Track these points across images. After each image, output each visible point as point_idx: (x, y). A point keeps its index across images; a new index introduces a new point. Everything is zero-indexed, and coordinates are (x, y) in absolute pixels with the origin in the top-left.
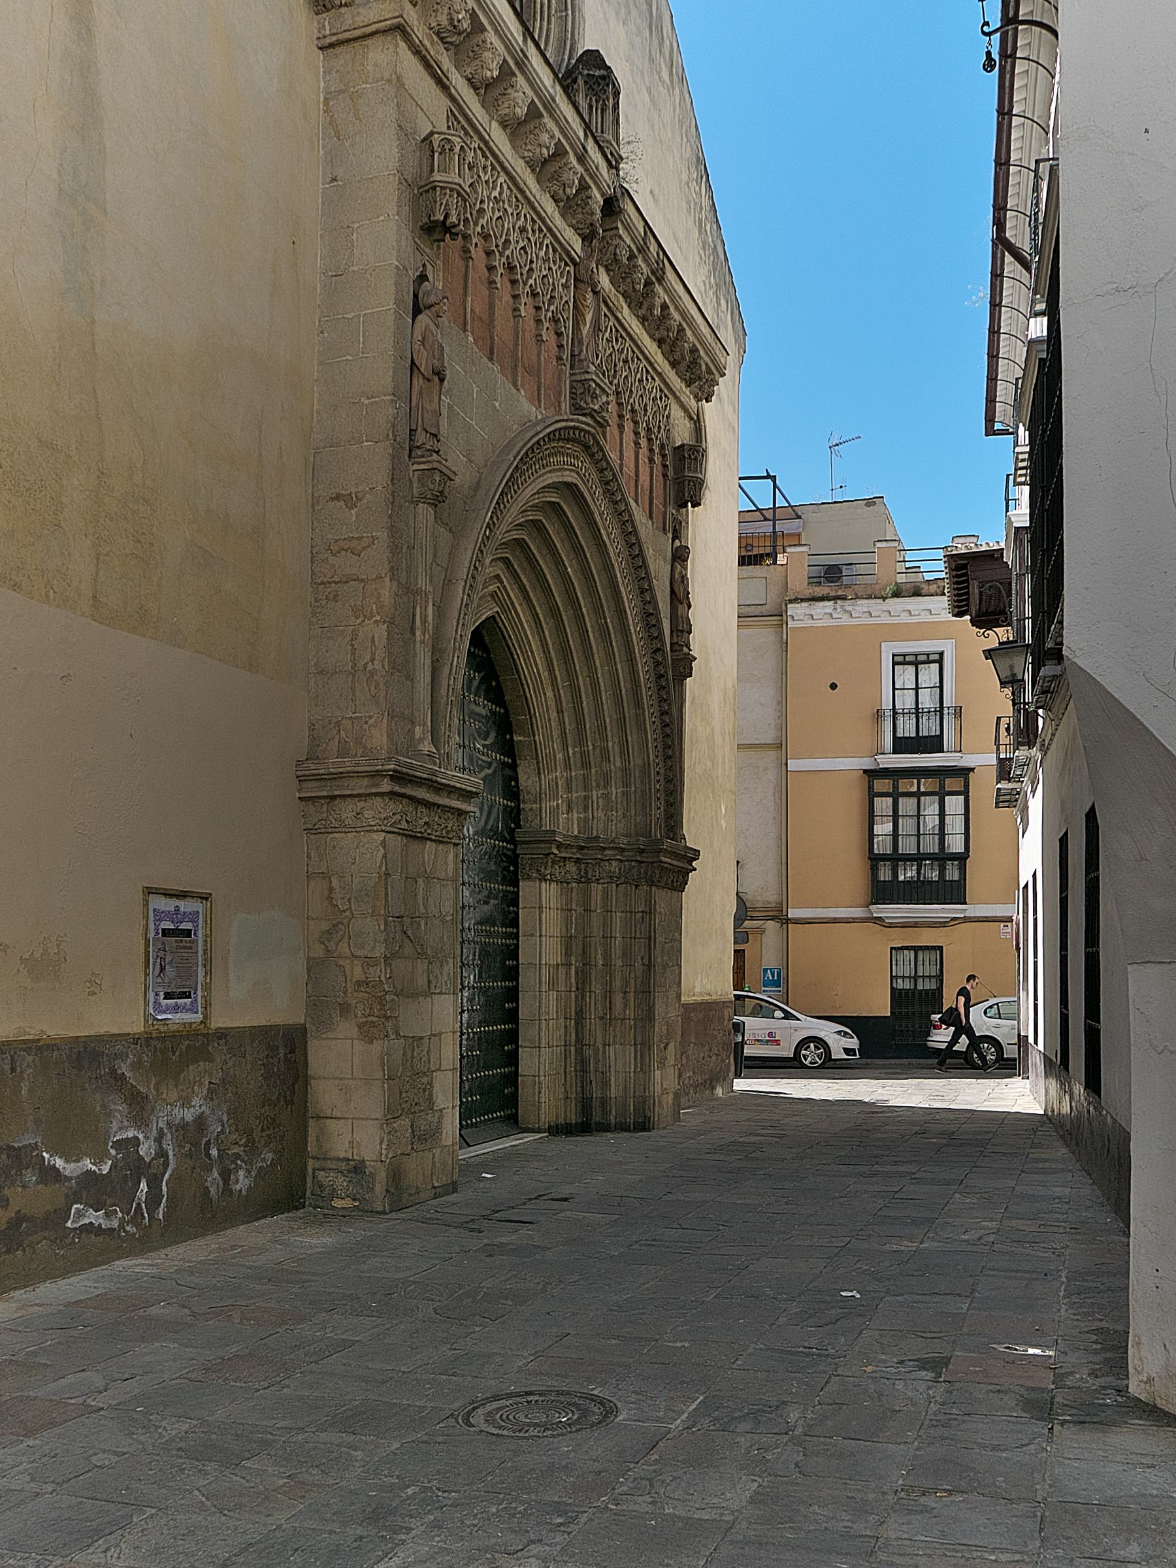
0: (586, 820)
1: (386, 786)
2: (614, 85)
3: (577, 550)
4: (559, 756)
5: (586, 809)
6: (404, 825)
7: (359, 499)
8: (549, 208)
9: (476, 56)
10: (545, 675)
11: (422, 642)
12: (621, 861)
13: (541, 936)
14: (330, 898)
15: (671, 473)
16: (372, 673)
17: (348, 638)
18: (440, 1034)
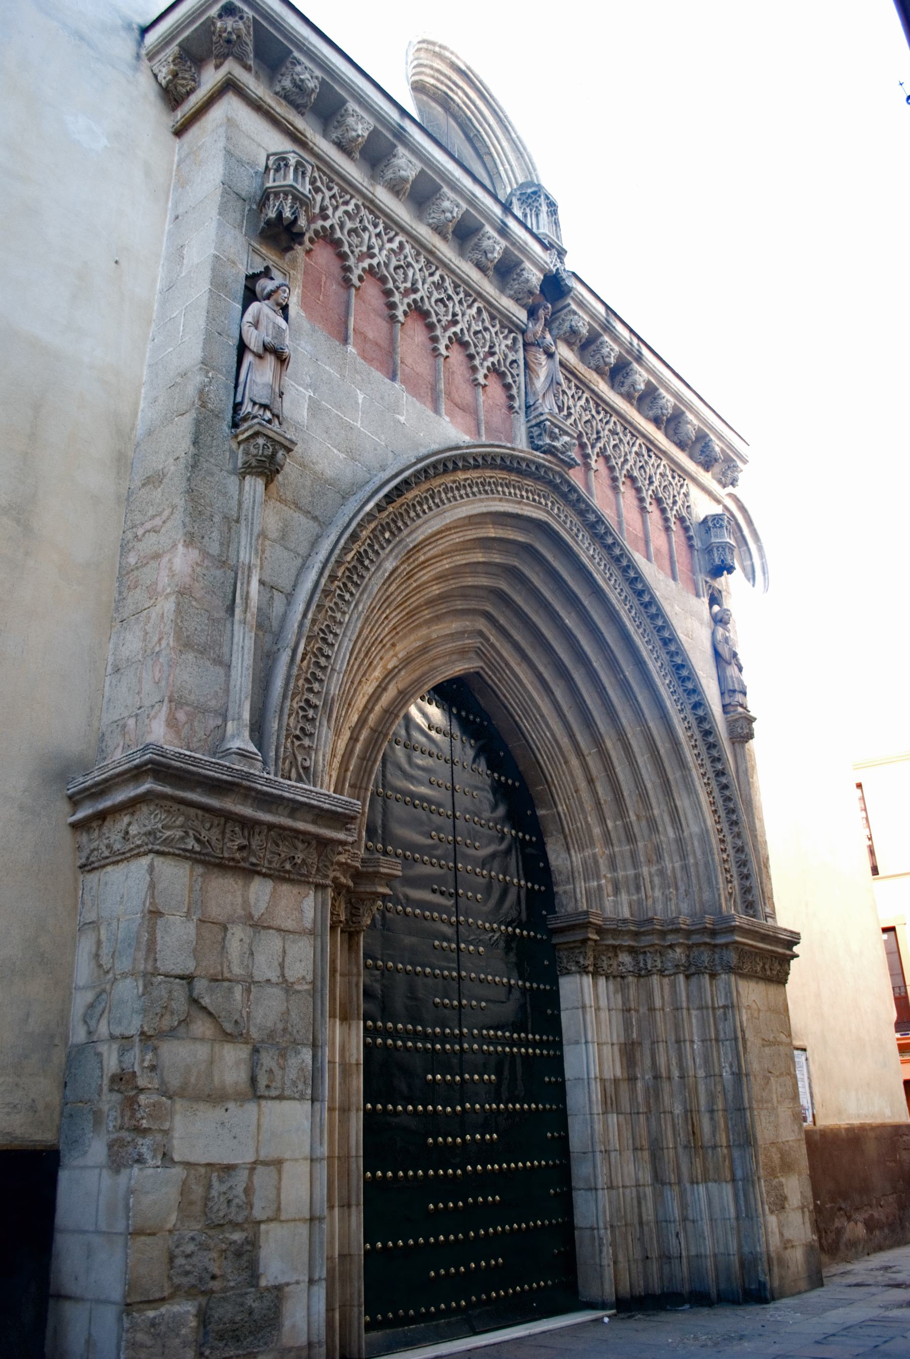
0: (640, 902)
2: (547, 198)
3: (573, 600)
4: (597, 831)
5: (638, 889)
6: (191, 843)
7: (164, 476)
8: (475, 275)
9: (341, 124)
11: (244, 622)
13: (586, 1042)
14: (97, 956)
15: (697, 543)
18: (278, 1163)
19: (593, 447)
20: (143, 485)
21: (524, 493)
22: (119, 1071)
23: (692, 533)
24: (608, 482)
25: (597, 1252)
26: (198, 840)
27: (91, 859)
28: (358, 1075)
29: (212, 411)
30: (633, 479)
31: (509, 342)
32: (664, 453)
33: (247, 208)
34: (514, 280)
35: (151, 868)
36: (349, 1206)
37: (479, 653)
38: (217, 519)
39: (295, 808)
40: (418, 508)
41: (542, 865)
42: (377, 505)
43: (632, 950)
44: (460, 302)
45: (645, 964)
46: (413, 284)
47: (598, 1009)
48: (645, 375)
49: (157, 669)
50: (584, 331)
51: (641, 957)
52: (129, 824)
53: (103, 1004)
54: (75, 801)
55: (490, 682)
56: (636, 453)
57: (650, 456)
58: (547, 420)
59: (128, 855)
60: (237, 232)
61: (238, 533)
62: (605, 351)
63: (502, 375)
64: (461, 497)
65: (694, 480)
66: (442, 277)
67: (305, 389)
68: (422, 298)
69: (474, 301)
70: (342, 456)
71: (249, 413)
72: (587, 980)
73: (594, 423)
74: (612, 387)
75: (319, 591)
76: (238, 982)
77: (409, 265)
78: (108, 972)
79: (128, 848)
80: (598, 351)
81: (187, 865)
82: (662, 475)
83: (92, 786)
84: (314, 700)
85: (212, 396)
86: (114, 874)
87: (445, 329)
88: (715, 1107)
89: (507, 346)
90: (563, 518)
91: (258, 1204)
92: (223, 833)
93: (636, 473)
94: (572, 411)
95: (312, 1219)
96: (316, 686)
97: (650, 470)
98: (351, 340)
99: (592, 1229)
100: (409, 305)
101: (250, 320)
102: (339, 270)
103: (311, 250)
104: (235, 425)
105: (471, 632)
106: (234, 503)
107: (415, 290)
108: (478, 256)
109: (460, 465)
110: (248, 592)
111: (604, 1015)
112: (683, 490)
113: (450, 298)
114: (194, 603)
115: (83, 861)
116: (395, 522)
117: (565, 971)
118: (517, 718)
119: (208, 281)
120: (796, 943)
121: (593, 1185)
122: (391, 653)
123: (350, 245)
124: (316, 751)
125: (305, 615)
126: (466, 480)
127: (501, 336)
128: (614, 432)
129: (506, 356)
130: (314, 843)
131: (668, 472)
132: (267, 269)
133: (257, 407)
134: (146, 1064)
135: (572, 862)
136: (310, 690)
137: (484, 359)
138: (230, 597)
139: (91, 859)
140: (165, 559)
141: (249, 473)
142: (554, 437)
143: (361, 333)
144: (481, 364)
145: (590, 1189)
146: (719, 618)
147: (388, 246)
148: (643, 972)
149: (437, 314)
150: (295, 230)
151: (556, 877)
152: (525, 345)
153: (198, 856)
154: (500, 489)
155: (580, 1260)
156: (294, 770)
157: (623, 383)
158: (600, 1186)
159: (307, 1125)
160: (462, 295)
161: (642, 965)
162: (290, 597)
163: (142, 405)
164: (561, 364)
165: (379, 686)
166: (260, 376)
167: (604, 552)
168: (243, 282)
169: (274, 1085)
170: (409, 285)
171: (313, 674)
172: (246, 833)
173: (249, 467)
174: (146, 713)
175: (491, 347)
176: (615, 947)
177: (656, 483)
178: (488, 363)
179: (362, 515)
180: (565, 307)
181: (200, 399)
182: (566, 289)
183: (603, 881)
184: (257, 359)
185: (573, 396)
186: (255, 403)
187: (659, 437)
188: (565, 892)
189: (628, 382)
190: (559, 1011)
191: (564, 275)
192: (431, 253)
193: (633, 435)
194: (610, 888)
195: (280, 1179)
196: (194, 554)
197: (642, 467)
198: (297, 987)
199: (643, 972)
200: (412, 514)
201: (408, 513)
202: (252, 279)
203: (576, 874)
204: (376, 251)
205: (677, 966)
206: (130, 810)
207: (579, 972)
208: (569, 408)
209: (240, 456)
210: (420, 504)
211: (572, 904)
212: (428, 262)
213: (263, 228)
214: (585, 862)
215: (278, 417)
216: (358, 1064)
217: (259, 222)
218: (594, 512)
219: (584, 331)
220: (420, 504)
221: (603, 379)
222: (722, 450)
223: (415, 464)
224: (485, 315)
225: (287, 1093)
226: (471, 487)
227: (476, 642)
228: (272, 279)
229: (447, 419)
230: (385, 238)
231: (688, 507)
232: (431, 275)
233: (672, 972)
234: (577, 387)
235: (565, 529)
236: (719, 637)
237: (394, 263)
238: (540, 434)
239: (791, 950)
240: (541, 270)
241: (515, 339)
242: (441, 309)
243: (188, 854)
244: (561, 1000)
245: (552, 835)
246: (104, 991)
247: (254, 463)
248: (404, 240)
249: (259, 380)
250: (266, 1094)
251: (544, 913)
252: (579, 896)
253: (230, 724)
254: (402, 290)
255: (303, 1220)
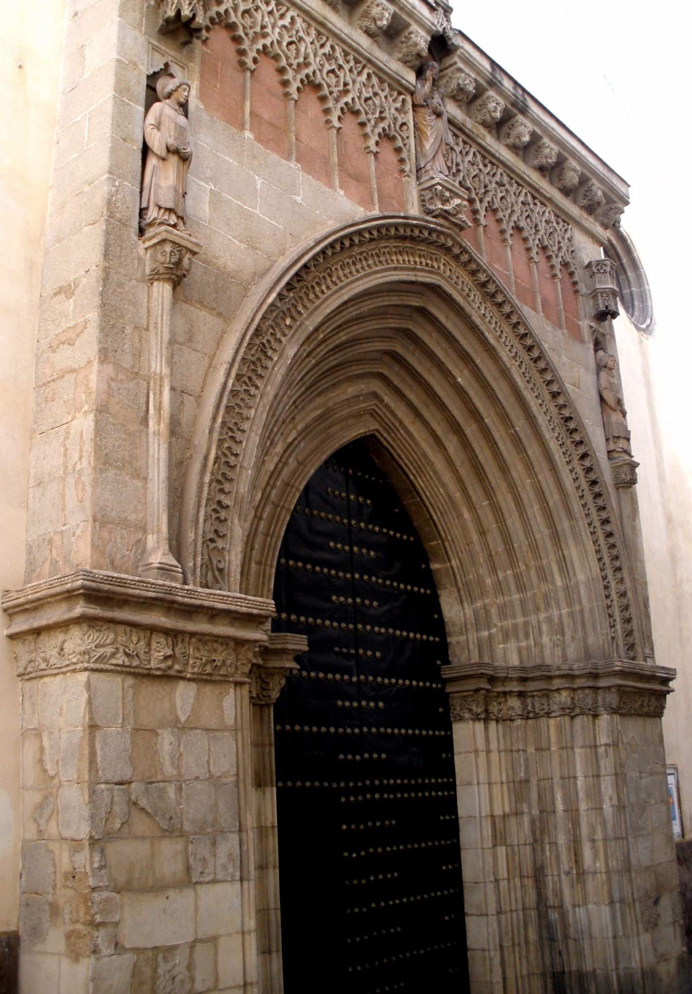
1: (80, 609)
5: (527, 636)
6: (120, 659)
7: (76, 286)
10: (458, 495)
12: (574, 690)
13: (478, 784)
14: (41, 761)
16: (80, 473)
17: (62, 439)
19: (481, 201)
20: (55, 294)
21: (417, 260)
22: (71, 869)
23: (576, 278)
24: (497, 235)
25: (488, 971)
26: (127, 655)
27: (29, 670)
28: (273, 835)
29: (120, 220)
30: (518, 229)
31: (398, 105)
32: (550, 200)
33: (146, 5)
34: (402, 43)
35: (88, 686)
36: (270, 953)
37: (373, 414)
38: (128, 330)
39: (213, 614)
40: (317, 289)
41: (436, 616)
42: (279, 294)
43: (521, 695)
44: (351, 70)
45: (533, 707)
46: (305, 58)
47: (488, 752)
48: (531, 127)
49: (80, 486)
50: (471, 88)
51: (529, 701)
52: (64, 641)
53: (51, 806)
54: (11, 612)
55: (385, 443)
56: (523, 203)
57: (535, 204)
58: (438, 184)
59: (64, 670)
60: (136, 33)
61: (148, 341)
62: (492, 105)
63: (392, 139)
64: (357, 271)
65: (578, 224)
66: (332, 47)
67: (207, 183)
68: (314, 72)
69: (364, 67)
70: (243, 246)
71: (155, 219)
72: (480, 726)
73: (482, 177)
74: (498, 138)
75: (227, 393)
76: (170, 782)
77: (301, 39)
78: (53, 778)
79: (64, 664)
80: (484, 105)
81: (119, 679)
82: (547, 222)
83: (26, 603)
84: (226, 501)
85: (119, 204)
86: (53, 684)
87: (337, 100)
88: (596, 837)
89: (396, 109)
90: (455, 279)
91: (199, 977)
92: (149, 644)
93: (522, 224)
94: (461, 168)
95: (245, 985)
96: (227, 486)
97: (535, 216)
98: (247, 126)
99: (484, 950)
100: (302, 81)
101: (153, 122)
102: (234, 54)
103: (207, 39)
104: (141, 232)
105: (366, 395)
106: (143, 312)
107: (307, 65)
108: (367, 23)
109: (357, 241)
110: (160, 403)
111: (494, 757)
112: (568, 235)
113: (340, 67)
114: (111, 420)
115: (21, 670)
116: (295, 306)
117: (458, 718)
118: (412, 477)
119: (112, 87)
120: (672, 679)
121: (484, 912)
122: (291, 426)
123: (244, 28)
124: (229, 552)
125: (214, 419)
126: (361, 253)
127: (390, 100)
128: (500, 184)
129: (396, 119)
130: (232, 644)
131: (553, 218)
132: (167, 65)
133: (162, 211)
134: (96, 865)
135: (465, 614)
136: (222, 491)
137: (375, 126)
138: (144, 408)
139: (29, 670)
140: (81, 376)
141: (157, 280)
142: (446, 201)
143: (257, 115)
144: (373, 131)
145: (482, 915)
146: (603, 364)
147: (280, 23)
148: (531, 715)
149: (329, 86)
150: (193, 26)
151: (449, 628)
152: (414, 106)
153: (128, 669)
154: (394, 258)
155: (472, 978)
156: (210, 574)
157: (509, 134)
158: (489, 913)
159: (237, 902)
160: (352, 63)
161: (530, 708)
162: (199, 399)
163: (50, 210)
164: (450, 122)
165: (280, 461)
166: (164, 179)
167: (495, 309)
168: (144, 82)
169: (207, 871)
170: (301, 60)
171: (224, 474)
172: (170, 643)
173: (157, 274)
174: (79, 553)
175: (381, 112)
176: (505, 693)
177: (542, 232)
178: (379, 130)
179: (265, 307)
180: (452, 65)
181: (108, 210)
182: (453, 48)
183: (494, 630)
184: (161, 161)
185: (461, 152)
186: (160, 208)
187: (543, 184)
188: (458, 643)
189: (514, 133)
190: (453, 754)
191: (451, 34)
192: (322, 24)
193: (519, 185)
194: (500, 636)
195: (216, 954)
196: (109, 369)
197: (528, 216)
198: (224, 780)
199: (531, 715)
200: (312, 296)
201: (307, 295)
202: (153, 78)
203: (469, 626)
204: (269, 30)
205: (562, 709)
206: (64, 629)
207: (473, 720)
208: (457, 165)
209: (148, 263)
210: (318, 284)
211: (466, 655)
212: (319, 34)
213: (162, 26)
214: (476, 613)
215: (182, 218)
216: (273, 827)
217: (157, 18)
218: (485, 271)
219: (471, 88)
220: (318, 284)
221: (490, 132)
222: (604, 194)
223: (312, 248)
224: (375, 80)
225: (220, 876)
226: (366, 260)
227: (371, 404)
228: (172, 76)
229: (342, 193)
230: (277, 14)
231: (573, 252)
232: (322, 46)
233: (557, 714)
234: (465, 143)
235: (458, 291)
236: (604, 382)
237: (287, 39)
238: (432, 198)
239: (667, 685)
240: (429, 31)
241: (404, 101)
242: (332, 80)
243: (119, 668)
244: (455, 745)
245: (446, 588)
246: (51, 793)
247: (162, 270)
248: (295, 14)
249: (163, 183)
250: (201, 880)
251: (439, 662)
252: (471, 647)
253: (150, 537)
254: (295, 66)
255: (237, 987)
